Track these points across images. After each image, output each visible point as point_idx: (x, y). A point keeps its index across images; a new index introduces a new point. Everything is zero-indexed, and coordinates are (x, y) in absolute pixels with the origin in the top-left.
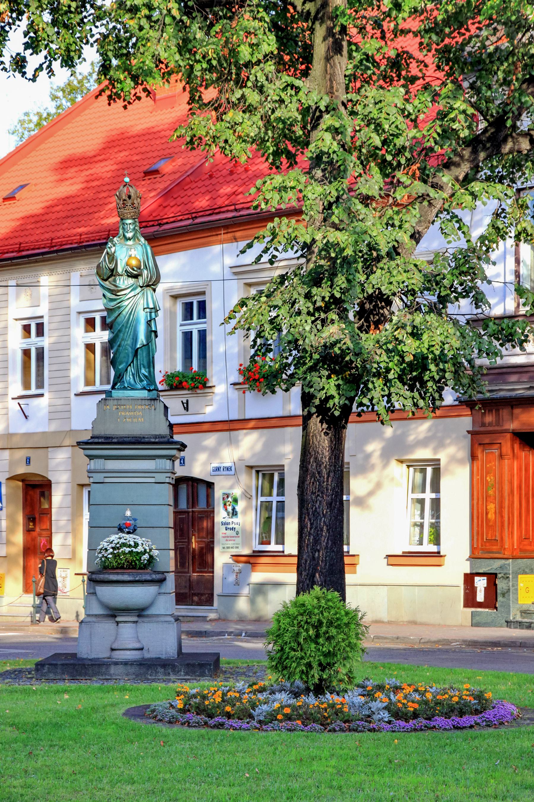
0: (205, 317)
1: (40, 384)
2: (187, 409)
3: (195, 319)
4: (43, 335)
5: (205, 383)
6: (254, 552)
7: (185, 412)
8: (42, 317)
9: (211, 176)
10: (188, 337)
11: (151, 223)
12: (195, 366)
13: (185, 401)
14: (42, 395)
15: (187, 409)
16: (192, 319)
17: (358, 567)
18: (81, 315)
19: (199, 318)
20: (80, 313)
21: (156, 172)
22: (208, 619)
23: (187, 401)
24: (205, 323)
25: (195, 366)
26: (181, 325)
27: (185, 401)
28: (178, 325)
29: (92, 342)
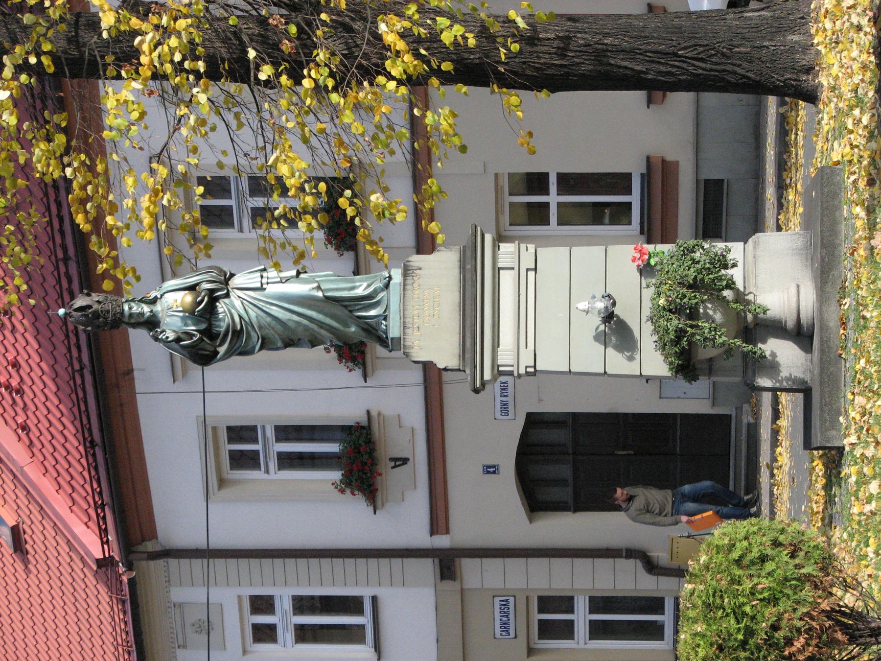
0: (254, 429)
1: (352, 605)
2: (405, 461)
3: (258, 447)
4: (271, 598)
5: (363, 428)
6: (642, 232)
7: (410, 463)
8: (239, 597)
9: (16, 365)
10: (288, 461)
11: (83, 408)
12: (333, 448)
13: (393, 464)
14: (374, 599)
15: (405, 461)
16: (257, 453)
17: (669, 158)
18: (249, 648)
19: (255, 441)
20: (245, 652)
21: (16, 532)
22: (752, 421)
23: (392, 459)
24: (264, 427)
25: (333, 448)
26: (267, 472)
27: (393, 464)
28: (266, 476)
29: (292, 629)
